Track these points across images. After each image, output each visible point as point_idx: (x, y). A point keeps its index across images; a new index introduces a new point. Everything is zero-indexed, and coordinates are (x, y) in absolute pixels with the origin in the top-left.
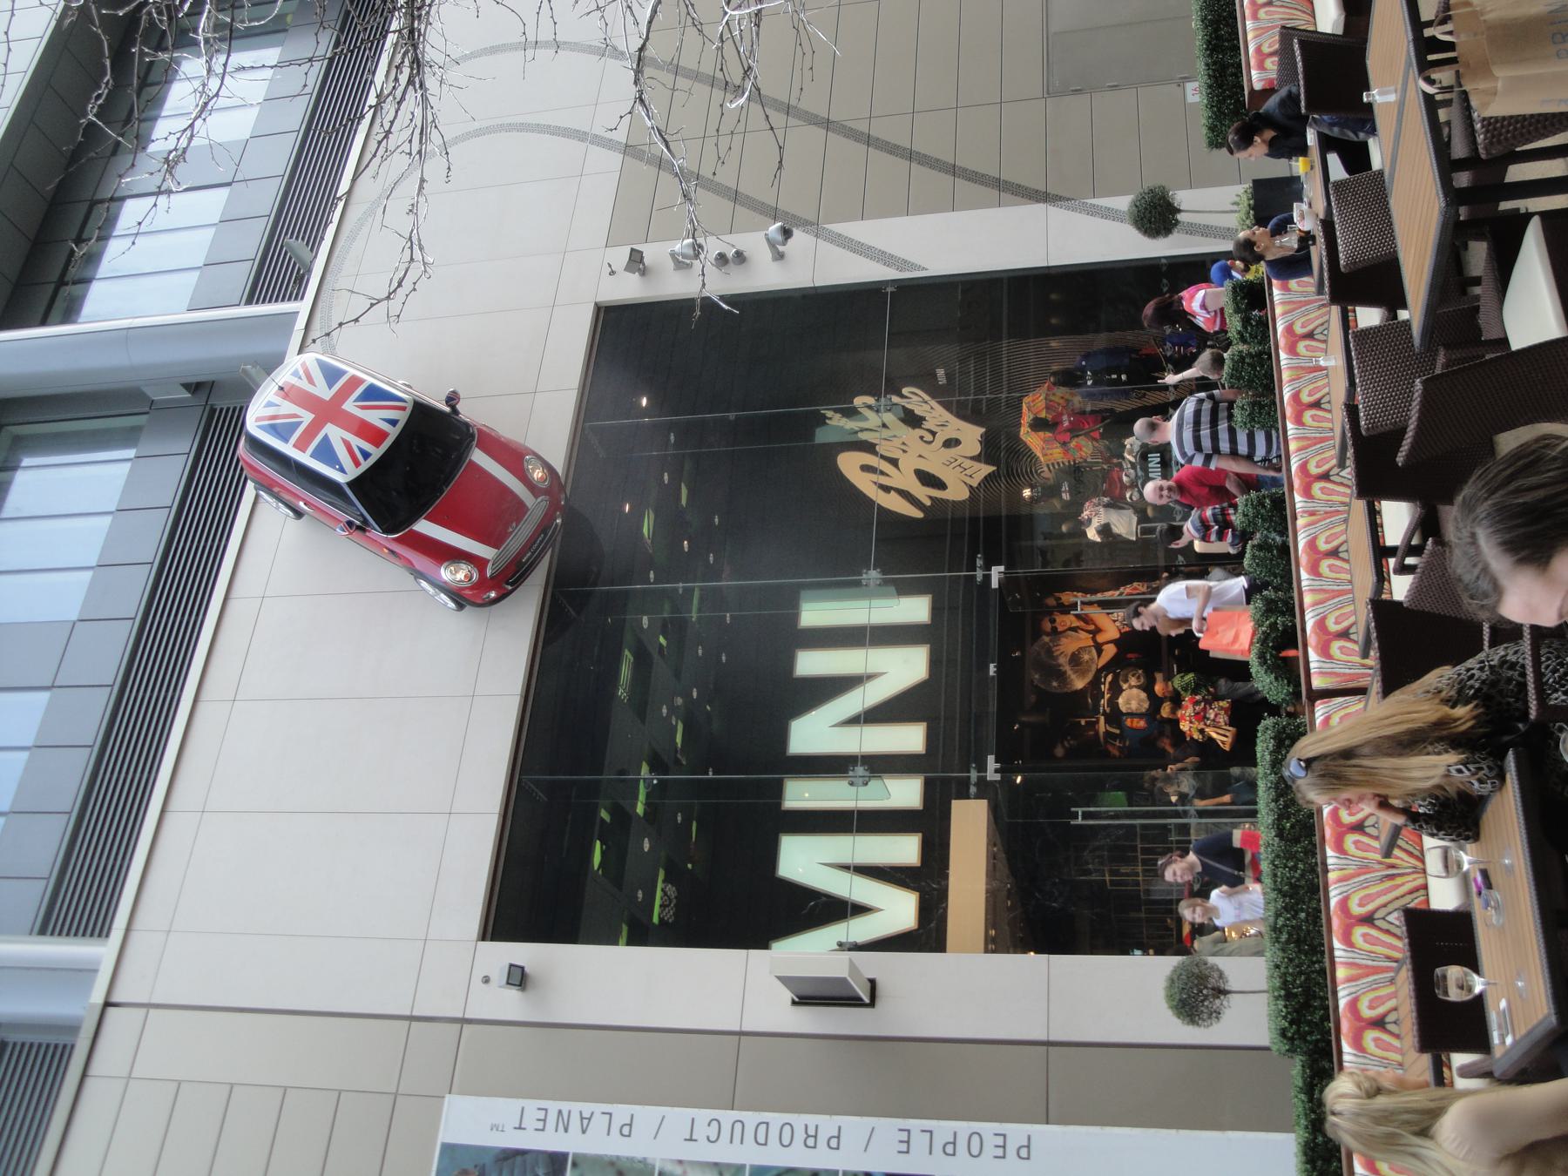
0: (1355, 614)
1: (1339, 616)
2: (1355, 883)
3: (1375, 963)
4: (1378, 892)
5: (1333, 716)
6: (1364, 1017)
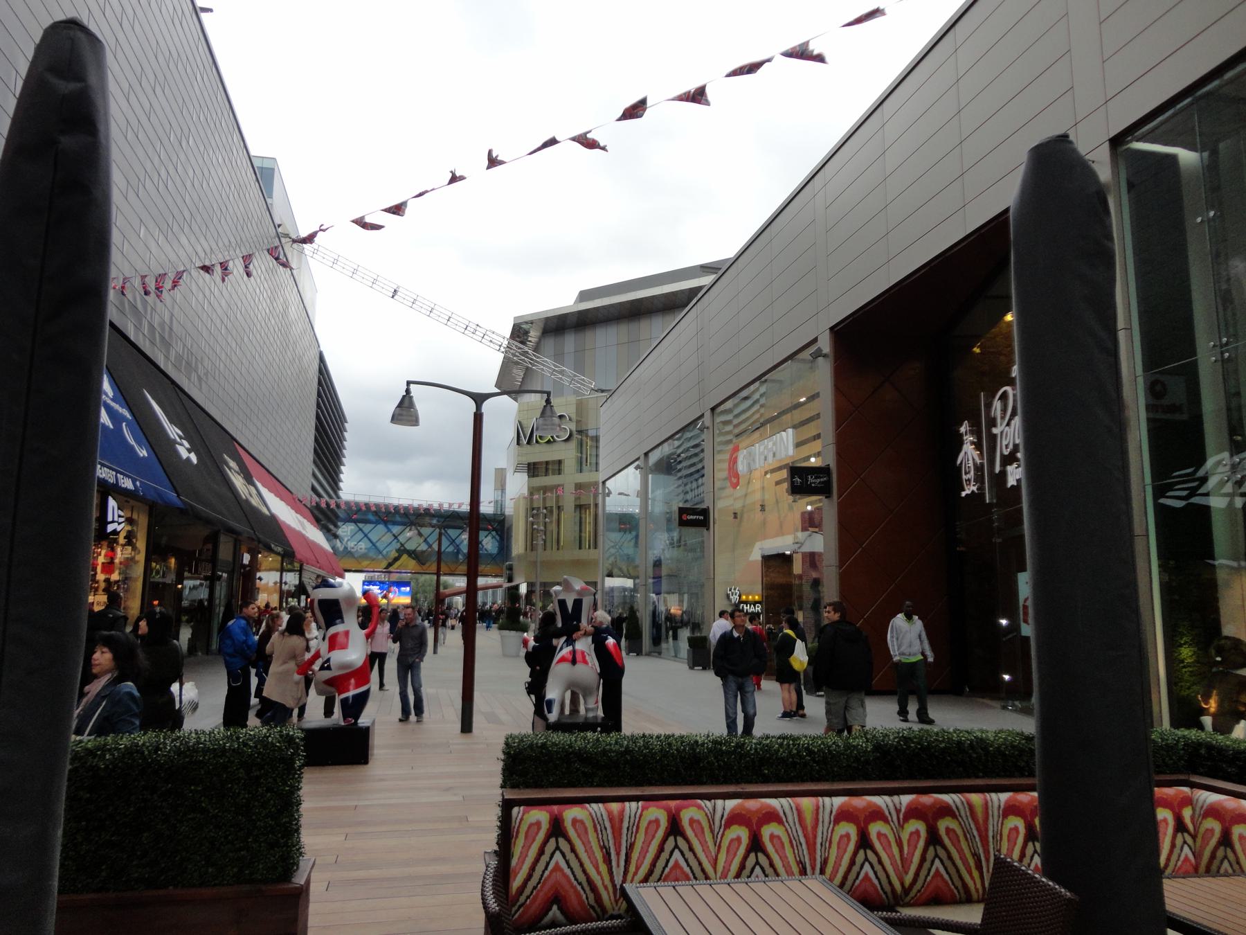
1: (957, 835)
2: (970, 825)
3: (818, 846)
4: (962, 850)
5: (955, 821)
6: (762, 829)
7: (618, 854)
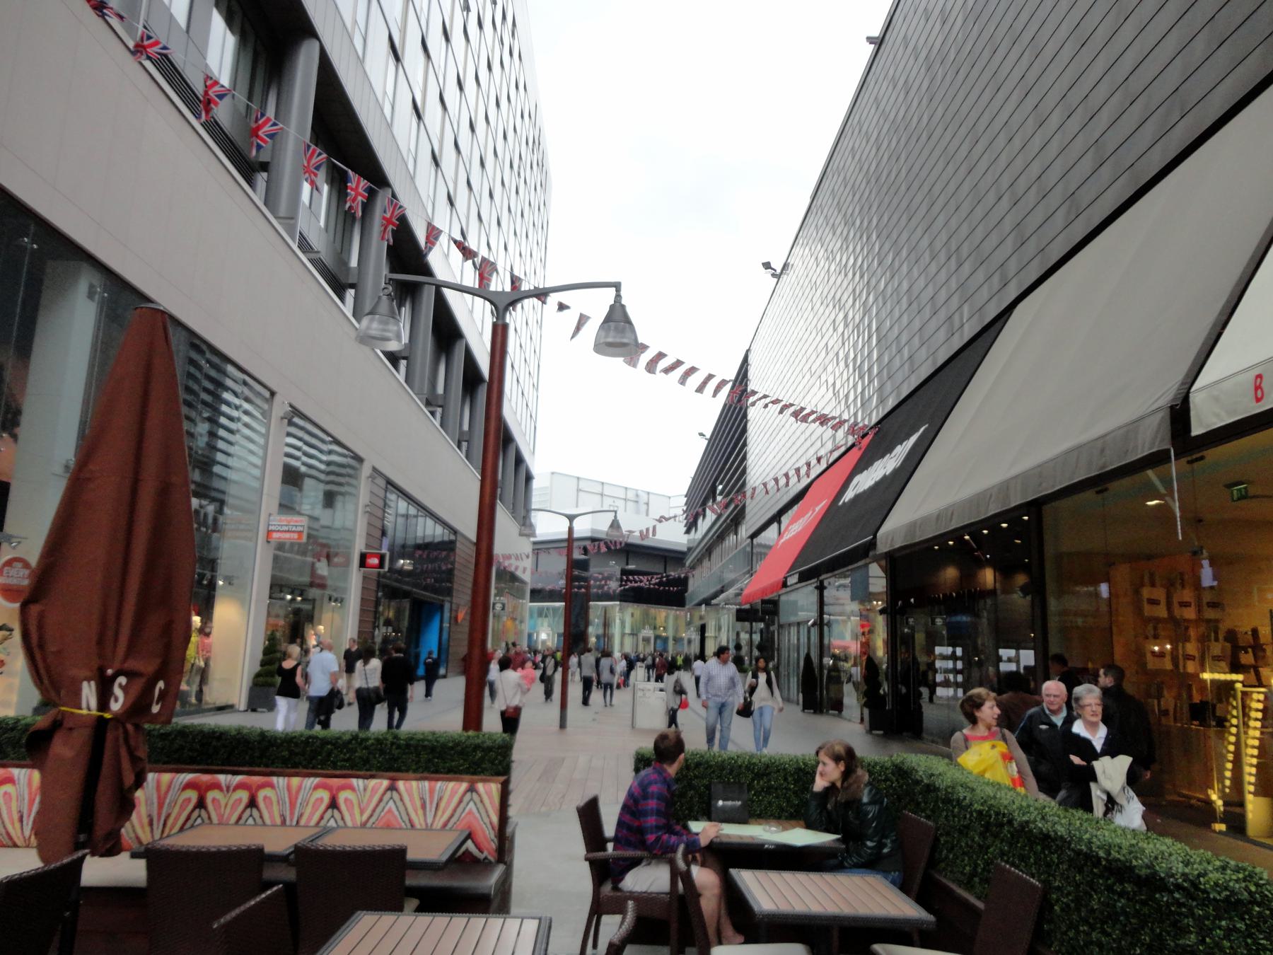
0: (219, 824)
3: (298, 805)
7: (431, 803)
